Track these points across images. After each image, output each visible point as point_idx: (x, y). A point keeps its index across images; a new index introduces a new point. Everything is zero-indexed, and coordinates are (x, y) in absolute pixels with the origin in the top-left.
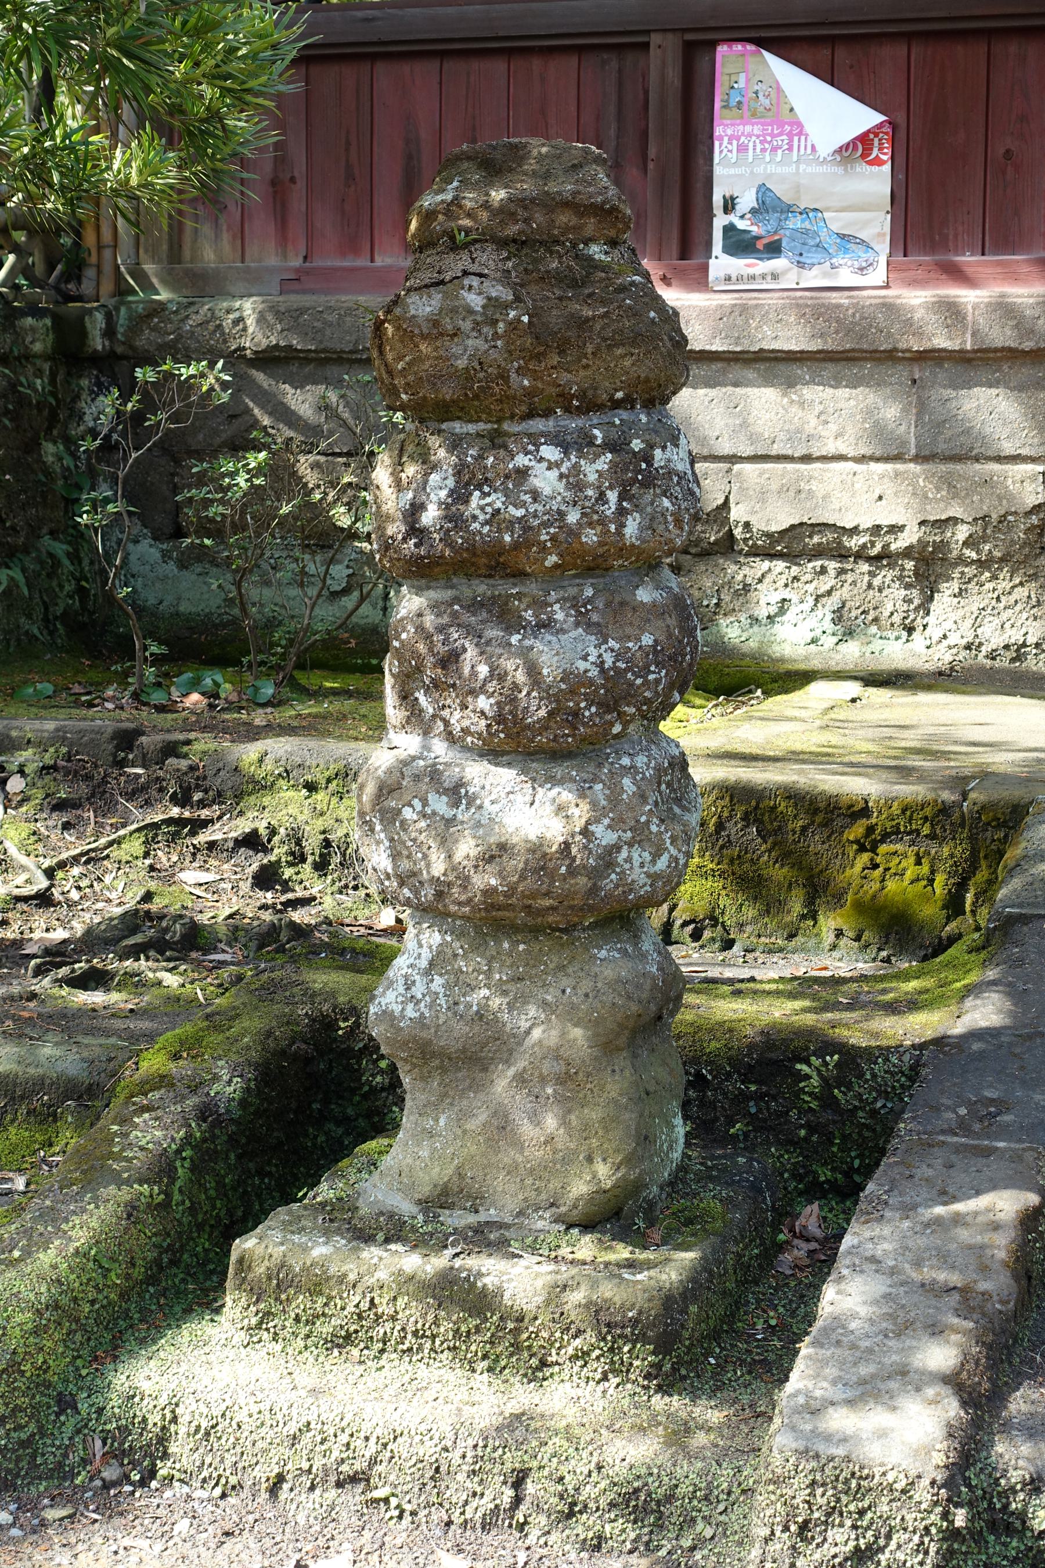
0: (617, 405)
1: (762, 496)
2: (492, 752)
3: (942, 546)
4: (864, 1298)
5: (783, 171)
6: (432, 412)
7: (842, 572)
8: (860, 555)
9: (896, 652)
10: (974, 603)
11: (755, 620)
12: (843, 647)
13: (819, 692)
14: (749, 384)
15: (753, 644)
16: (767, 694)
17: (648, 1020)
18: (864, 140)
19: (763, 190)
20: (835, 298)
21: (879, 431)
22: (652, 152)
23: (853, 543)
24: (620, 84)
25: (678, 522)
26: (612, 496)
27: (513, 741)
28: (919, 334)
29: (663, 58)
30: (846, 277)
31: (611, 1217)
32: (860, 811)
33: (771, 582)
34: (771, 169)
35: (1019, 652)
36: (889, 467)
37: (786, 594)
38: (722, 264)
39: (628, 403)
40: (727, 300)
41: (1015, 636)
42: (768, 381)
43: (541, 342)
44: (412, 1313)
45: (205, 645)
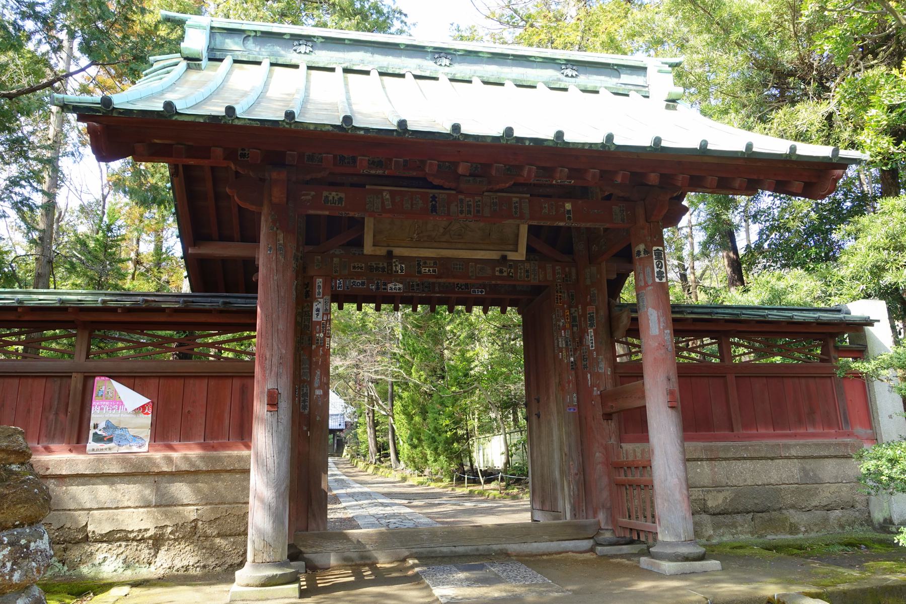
0: (16, 526)
1: (100, 522)
3: (163, 534)
4: (297, 111)
5: (115, 416)
7: (127, 545)
8: (133, 540)
9: (145, 572)
10: (172, 553)
11: (94, 565)
12: (126, 572)
14: (98, 484)
15: (92, 574)
16: (95, 594)
18: (143, 407)
19: (108, 422)
20: (130, 456)
21: (143, 498)
22: (69, 409)
23: (131, 536)
24: (60, 387)
25: (39, 571)
26: (9, 565)
28: (158, 466)
29: (76, 382)
30: (135, 449)
33: (101, 551)
34: (111, 415)
35: (187, 568)
36: (145, 509)
37: (106, 555)
38: (91, 445)
39: (22, 525)
40: (92, 457)
41: (185, 563)
42: (104, 483)
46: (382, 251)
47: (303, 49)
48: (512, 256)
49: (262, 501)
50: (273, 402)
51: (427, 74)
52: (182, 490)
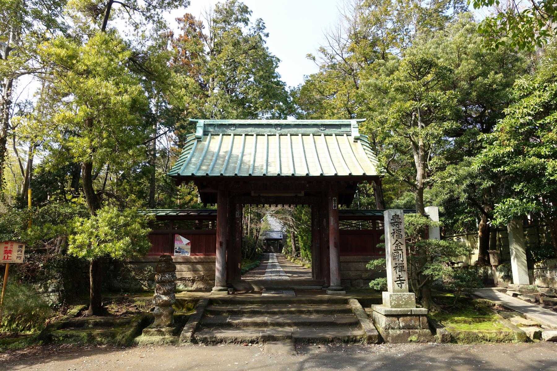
2: (162, 294)
5: (181, 246)
6: (160, 272)
9: (190, 289)
13: (183, 292)
17: (172, 313)
27: (164, 294)
31: (169, 326)
32: (186, 300)
38: (175, 254)
43: (167, 268)
44: (156, 332)
45: (126, 290)
46: (257, 195)
47: (232, 128)
48: (299, 195)
49: (218, 270)
50: (221, 244)
51: (272, 134)
52: (199, 267)
